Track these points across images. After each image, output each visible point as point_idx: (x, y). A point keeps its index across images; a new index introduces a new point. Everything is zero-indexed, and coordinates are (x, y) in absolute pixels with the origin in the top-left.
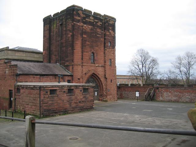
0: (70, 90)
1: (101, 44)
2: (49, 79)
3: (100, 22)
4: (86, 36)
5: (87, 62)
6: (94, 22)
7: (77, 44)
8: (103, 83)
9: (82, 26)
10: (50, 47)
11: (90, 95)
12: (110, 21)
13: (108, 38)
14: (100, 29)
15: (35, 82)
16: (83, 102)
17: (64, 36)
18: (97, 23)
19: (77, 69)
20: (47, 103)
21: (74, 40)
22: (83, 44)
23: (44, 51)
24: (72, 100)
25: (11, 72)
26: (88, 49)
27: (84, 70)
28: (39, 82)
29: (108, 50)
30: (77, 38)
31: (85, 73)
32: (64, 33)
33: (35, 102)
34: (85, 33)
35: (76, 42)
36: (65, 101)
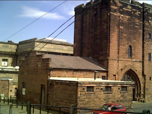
0: (108, 88)
1: (139, 36)
2: (82, 74)
3: (139, 11)
4: (122, 28)
5: (123, 56)
6: (131, 12)
7: (113, 36)
8: (140, 81)
9: (119, 17)
10: (81, 39)
11: (128, 94)
12: (150, 10)
13: (147, 29)
14: (139, 19)
15: (68, 77)
16: (121, 101)
17: (99, 27)
18: (136, 13)
19: (112, 64)
20: (83, 101)
21: (111, 32)
22: (120, 37)
23: (75, 44)
24: (109, 99)
25: (44, 66)
26: (125, 42)
27: (120, 65)
28: (73, 77)
29: (147, 43)
30: (113, 30)
31: (121, 69)
32: (99, 24)
33: (71, 99)
34: (122, 24)
35: (112, 34)
36: (102, 100)
